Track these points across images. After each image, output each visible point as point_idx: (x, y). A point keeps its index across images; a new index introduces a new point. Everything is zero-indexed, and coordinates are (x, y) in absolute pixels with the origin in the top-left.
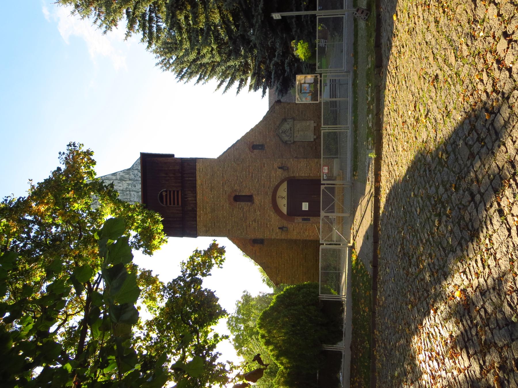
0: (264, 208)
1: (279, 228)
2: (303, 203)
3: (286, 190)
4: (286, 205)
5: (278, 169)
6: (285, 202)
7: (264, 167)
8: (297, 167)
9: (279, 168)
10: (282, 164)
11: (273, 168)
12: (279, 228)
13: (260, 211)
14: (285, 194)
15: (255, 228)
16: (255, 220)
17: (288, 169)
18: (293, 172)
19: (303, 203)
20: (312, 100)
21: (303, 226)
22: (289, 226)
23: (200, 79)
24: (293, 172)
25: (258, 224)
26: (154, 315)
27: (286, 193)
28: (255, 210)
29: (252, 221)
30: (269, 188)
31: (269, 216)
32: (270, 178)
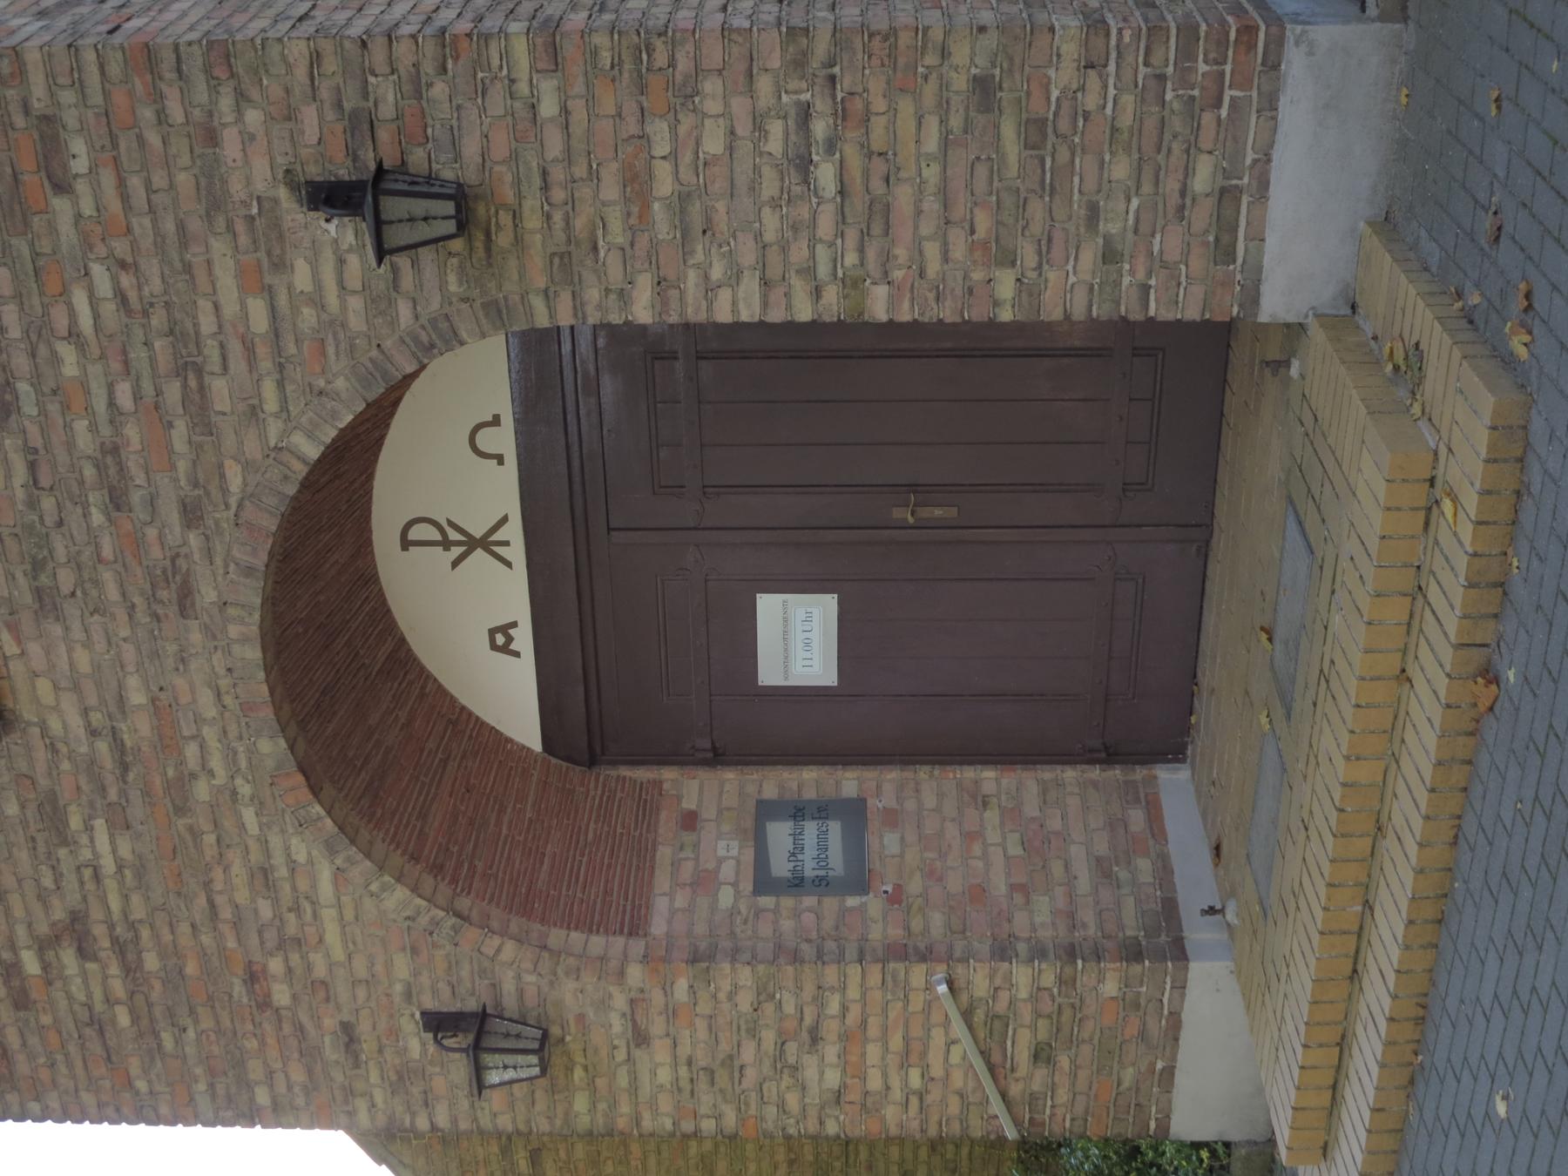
0: (180, 786)
1: (438, 1023)
2: (768, 605)
3: (504, 440)
4: (524, 639)
5: (293, 213)
6: (505, 590)
7: (62, 187)
8: (637, 184)
9: (331, 197)
10: (362, 124)
11: (214, 201)
12: (438, 1023)
13: (120, 822)
14: (493, 495)
15: (99, 1025)
16: (76, 929)
17: (465, 207)
18: (564, 265)
19: (768, 605)
20: (658, 784)
21: (764, 993)
22: (571, 996)
23: (1432, 294)
24: (564, 265)
25: (131, 970)
26: (259, 457)
27: (509, 474)
28: (52, 813)
29: (43, 946)
30: (192, 515)
31: (263, 876)
32: (189, 368)
